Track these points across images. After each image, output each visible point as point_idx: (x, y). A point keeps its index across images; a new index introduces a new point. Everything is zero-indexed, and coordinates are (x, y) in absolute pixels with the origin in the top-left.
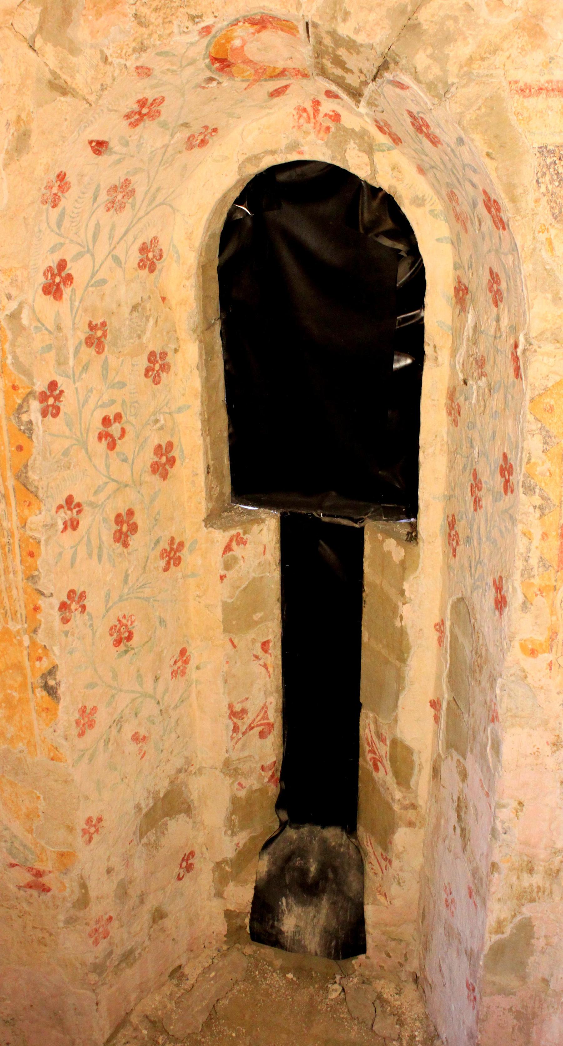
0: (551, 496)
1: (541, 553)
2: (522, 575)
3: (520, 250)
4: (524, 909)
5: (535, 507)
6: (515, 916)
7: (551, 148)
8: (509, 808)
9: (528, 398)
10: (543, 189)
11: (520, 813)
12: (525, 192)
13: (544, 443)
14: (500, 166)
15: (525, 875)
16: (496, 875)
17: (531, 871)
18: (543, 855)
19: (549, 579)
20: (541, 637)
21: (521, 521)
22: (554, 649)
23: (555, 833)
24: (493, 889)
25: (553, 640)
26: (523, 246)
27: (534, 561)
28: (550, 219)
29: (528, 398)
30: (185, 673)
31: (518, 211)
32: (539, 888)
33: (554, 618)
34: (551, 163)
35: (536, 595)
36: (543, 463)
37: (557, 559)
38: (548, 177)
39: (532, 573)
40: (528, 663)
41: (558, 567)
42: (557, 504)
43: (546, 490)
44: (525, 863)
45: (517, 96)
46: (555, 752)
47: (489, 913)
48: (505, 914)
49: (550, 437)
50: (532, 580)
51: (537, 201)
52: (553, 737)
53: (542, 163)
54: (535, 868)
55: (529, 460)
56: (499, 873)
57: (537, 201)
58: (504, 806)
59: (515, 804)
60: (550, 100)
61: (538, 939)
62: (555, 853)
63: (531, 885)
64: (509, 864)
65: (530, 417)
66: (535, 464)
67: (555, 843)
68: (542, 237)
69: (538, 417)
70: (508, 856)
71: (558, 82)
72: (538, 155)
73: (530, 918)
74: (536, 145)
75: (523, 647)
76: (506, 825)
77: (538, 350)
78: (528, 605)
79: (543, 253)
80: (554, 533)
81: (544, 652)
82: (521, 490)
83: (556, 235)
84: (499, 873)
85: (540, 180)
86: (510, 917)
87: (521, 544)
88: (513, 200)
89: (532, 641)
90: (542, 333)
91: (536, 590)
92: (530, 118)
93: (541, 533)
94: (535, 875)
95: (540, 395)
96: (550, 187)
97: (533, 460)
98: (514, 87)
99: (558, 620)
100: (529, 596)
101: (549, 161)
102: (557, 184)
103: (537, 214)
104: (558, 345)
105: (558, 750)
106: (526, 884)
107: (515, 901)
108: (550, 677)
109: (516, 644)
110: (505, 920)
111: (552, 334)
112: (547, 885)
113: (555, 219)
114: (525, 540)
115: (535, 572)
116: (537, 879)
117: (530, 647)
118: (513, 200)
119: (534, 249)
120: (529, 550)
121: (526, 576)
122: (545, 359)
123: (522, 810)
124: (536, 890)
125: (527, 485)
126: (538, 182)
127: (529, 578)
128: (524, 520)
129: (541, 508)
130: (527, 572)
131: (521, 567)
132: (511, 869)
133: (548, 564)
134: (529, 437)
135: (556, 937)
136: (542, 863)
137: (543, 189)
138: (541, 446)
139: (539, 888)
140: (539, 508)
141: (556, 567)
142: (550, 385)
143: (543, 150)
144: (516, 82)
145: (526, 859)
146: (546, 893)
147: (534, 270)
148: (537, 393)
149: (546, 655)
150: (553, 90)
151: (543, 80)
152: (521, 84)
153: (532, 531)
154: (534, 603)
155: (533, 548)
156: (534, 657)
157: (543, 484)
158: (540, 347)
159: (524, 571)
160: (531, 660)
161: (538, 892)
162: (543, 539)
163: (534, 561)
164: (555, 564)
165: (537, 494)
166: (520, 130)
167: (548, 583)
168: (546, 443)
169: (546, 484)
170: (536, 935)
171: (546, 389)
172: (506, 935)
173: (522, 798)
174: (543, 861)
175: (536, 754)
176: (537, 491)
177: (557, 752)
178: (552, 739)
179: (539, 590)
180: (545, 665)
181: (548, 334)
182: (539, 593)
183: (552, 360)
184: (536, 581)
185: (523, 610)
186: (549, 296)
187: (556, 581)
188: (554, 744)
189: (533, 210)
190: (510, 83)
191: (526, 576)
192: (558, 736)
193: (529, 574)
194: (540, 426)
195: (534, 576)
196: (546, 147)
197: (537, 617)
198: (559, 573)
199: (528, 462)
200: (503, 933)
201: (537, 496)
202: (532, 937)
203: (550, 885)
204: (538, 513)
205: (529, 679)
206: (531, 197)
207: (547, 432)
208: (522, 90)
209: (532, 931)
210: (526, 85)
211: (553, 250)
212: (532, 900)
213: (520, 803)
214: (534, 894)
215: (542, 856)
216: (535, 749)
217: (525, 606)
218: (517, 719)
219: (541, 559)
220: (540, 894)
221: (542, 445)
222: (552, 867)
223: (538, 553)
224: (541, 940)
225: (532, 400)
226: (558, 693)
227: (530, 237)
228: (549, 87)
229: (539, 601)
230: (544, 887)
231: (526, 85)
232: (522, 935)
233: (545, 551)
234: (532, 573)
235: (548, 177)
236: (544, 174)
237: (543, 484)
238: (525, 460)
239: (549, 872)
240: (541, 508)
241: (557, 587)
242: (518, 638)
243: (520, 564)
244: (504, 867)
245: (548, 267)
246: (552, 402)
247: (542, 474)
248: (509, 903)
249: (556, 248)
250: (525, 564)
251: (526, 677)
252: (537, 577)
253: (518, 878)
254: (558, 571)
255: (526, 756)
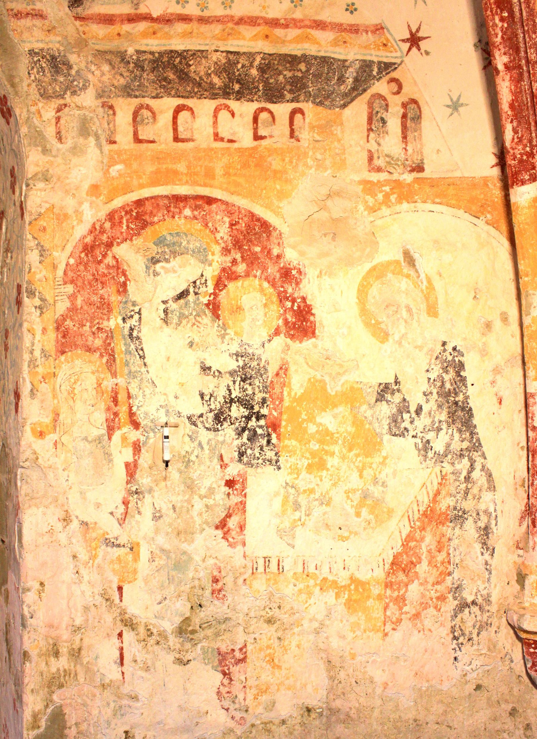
0: (48, 298)
1: (43, 346)
2: (29, 366)
3: (18, 118)
4: (55, 697)
5: (36, 307)
6: (47, 706)
7: (37, 51)
8: (33, 591)
9: (27, 222)
10: (33, 77)
11: (42, 594)
12: (22, 80)
13: (40, 256)
14: (4, 64)
15: (52, 659)
16: (28, 664)
17: (57, 654)
18: (65, 635)
19: (50, 367)
20: (47, 420)
21: (26, 320)
22: (58, 429)
23: (73, 610)
24: (26, 681)
25: (56, 421)
26: (20, 115)
27: (37, 353)
28: (38, 96)
29: (27, 222)
30: (123, 503)
31: (16, 93)
32: (65, 671)
33: (56, 401)
34: (37, 61)
35: (41, 382)
36: (41, 271)
37: (54, 349)
38: (35, 70)
39: (37, 364)
40: (38, 445)
41: (56, 355)
42: (52, 303)
43: (44, 293)
44: (51, 647)
45: (13, 19)
46: (65, 527)
47: (24, 708)
48: (39, 706)
49: (44, 251)
50: (37, 369)
51: (29, 85)
52: (63, 512)
53: (31, 61)
54: (61, 651)
55: (30, 270)
56: (31, 663)
57: (29, 85)
58: (29, 590)
59: (37, 586)
60: (34, 21)
61: (70, 728)
62: (75, 631)
63: (58, 670)
64: (38, 650)
65: (29, 237)
66: (34, 272)
67: (74, 621)
68: (33, 109)
69: (35, 236)
70: (36, 641)
71: (39, 10)
72: (28, 55)
73: (61, 706)
74: (26, 49)
75: (33, 430)
76: (32, 608)
77: (34, 187)
78: (35, 392)
79: (35, 120)
80: (51, 327)
81: (50, 433)
82: (25, 294)
83: (43, 107)
84: (31, 663)
85: (31, 72)
86: (43, 708)
87: (27, 339)
88: (13, 85)
89: (40, 424)
90: (36, 174)
91: (40, 377)
92: (22, 32)
93: (41, 328)
94: (60, 659)
95: (36, 219)
96: (37, 76)
97: (33, 270)
98: (10, 13)
99: (59, 402)
100: (35, 383)
101: (35, 59)
102: (41, 74)
103: (30, 95)
104: (47, 183)
105: (67, 525)
106: (54, 670)
107: (46, 689)
108: (56, 456)
109: (28, 428)
110: (39, 712)
111: (43, 175)
112: (72, 667)
113: (42, 96)
114: (30, 336)
115: (39, 362)
116: (63, 663)
117: (39, 429)
118: (13, 85)
119: (28, 118)
120: (33, 345)
121: (32, 366)
122: (39, 192)
123: (43, 590)
124: (63, 675)
125: (29, 290)
126: (29, 73)
127: (34, 367)
128: (28, 319)
129: (40, 308)
130: (33, 363)
131: (28, 359)
132: (40, 655)
133: (48, 354)
134: (29, 251)
135: (85, 724)
136: (66, 644)
137: (33, 77)
138: (38, 258)
139: (65, 671)
140: (39, 308)
141: (54, 356)
142: (43, 211)
143: (32, 52)
144: (12, 10)
145: (51, 642)
146: (72, 676)
147: (29, 132)
148: (34, 218)
149: (52, 435)
150: (36, 15)
151: (29, 8)
152: (15, 11)
153: (34, 327)
154: (39, 390)
155: (36, 341)
156: (42, 438)
157: (41, 288)
158: (35, 185)
159: (30, 362)
160: (40, 442)
161: (65, 676)
162: (43, 333)
163: (37, 353)
164: (53, 353)
165: (37, 297)
166: (16, 41)
167: (49, 371)
168: (41, 255)
169: (43, 288)
170: (68, 724)
171: (40, 215)
172: (42, 730)
173: (43, 578)
174: (66, 641)
175: (51, 532)
176: (37, 294)
177: (68, 527)
178: (62, 515)
179: (43, 377)
180: (51, 445)
181: (40, 176)
182: (42, 380)
183: (43, 193)
184: (40, 370)
185: (31, 397)
186: (40, 149)
187: (55, 368)
188: (64, 520)
189: (27, 92)
190: (8, 10)
191: (32, 366)
192: (67, 511)
193: (34, 364)
194: (36, 242)
195: (38, 366)
196: (33, 50)
197: (42, 401)
198: (57, 361)
199: (29, 272)
200: (39, 727)
201: (37, 299)
202: (65, 727)
203: (75, 667)
204: (39, 312)
205: (40, 461)
206: (25, 84)
207: (42, 246)
208: (16, 15)
209: (64, 721)
210: (18, 11)
211: (41, 116)
212: (61, 686)
213: (42, 584)
214: (62, 680)
215: (65, 637)
216: (50, 527)
217: (33, 393)
218: (33, 500)
219: (43, 351)
220: (67, 678)
221: (38, 257)
222: (74, 646)
223: (40, 347)
224: (72, 729)
225: (30, 223)
226: (63, 470)
227: (25, 110)
228: (34, 13)
229: (43, 387)
230: (70, 670)
231: (18, 11)
232: (56, 726)
233: (46, 343)
234: (37, 364)
235: (35, 70)
236: (33, 68)
237: (41, 288)
238: (27, 270)
239: (72, 653)
240: (40, 308)
241: (56, 374)
242: (29, 422)
243: (26, 357)
244: (34, 653)
245: (38, 129)
246: (45, 224)
247: (40, 280)
248: (41, 692)
249: (43, 115)
250: (31, 356)
251: (37, 458)
252: (40, 366)
253: (47, 664)
254: (56, 359)
255: (43, 535)
